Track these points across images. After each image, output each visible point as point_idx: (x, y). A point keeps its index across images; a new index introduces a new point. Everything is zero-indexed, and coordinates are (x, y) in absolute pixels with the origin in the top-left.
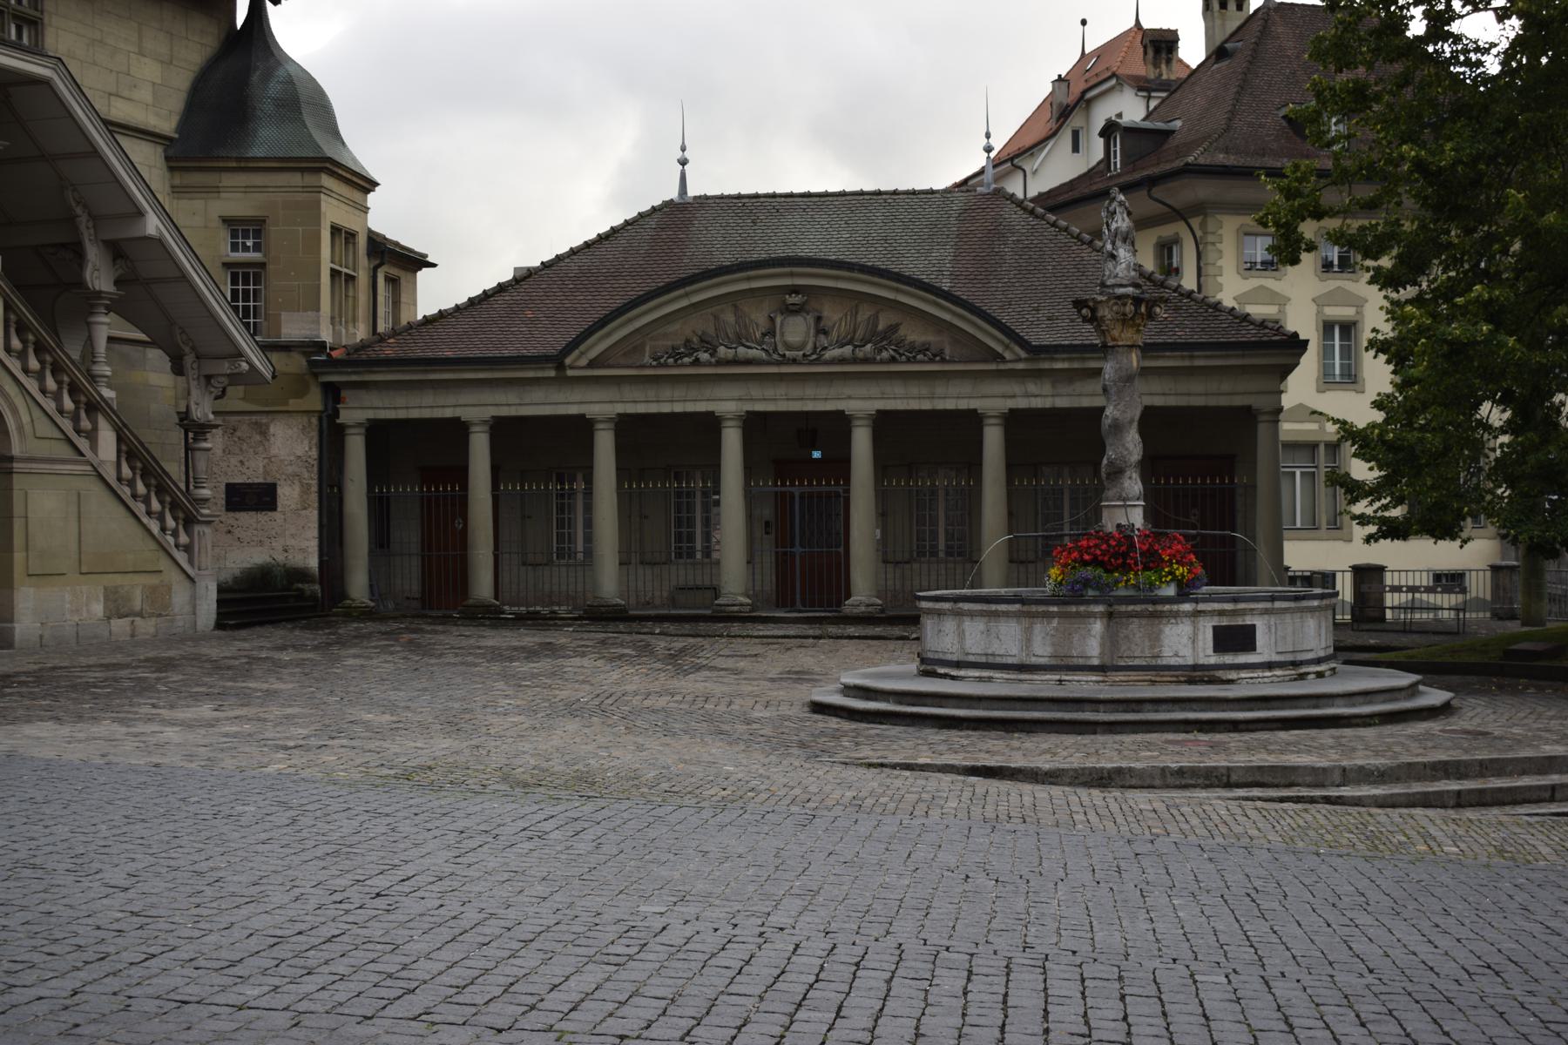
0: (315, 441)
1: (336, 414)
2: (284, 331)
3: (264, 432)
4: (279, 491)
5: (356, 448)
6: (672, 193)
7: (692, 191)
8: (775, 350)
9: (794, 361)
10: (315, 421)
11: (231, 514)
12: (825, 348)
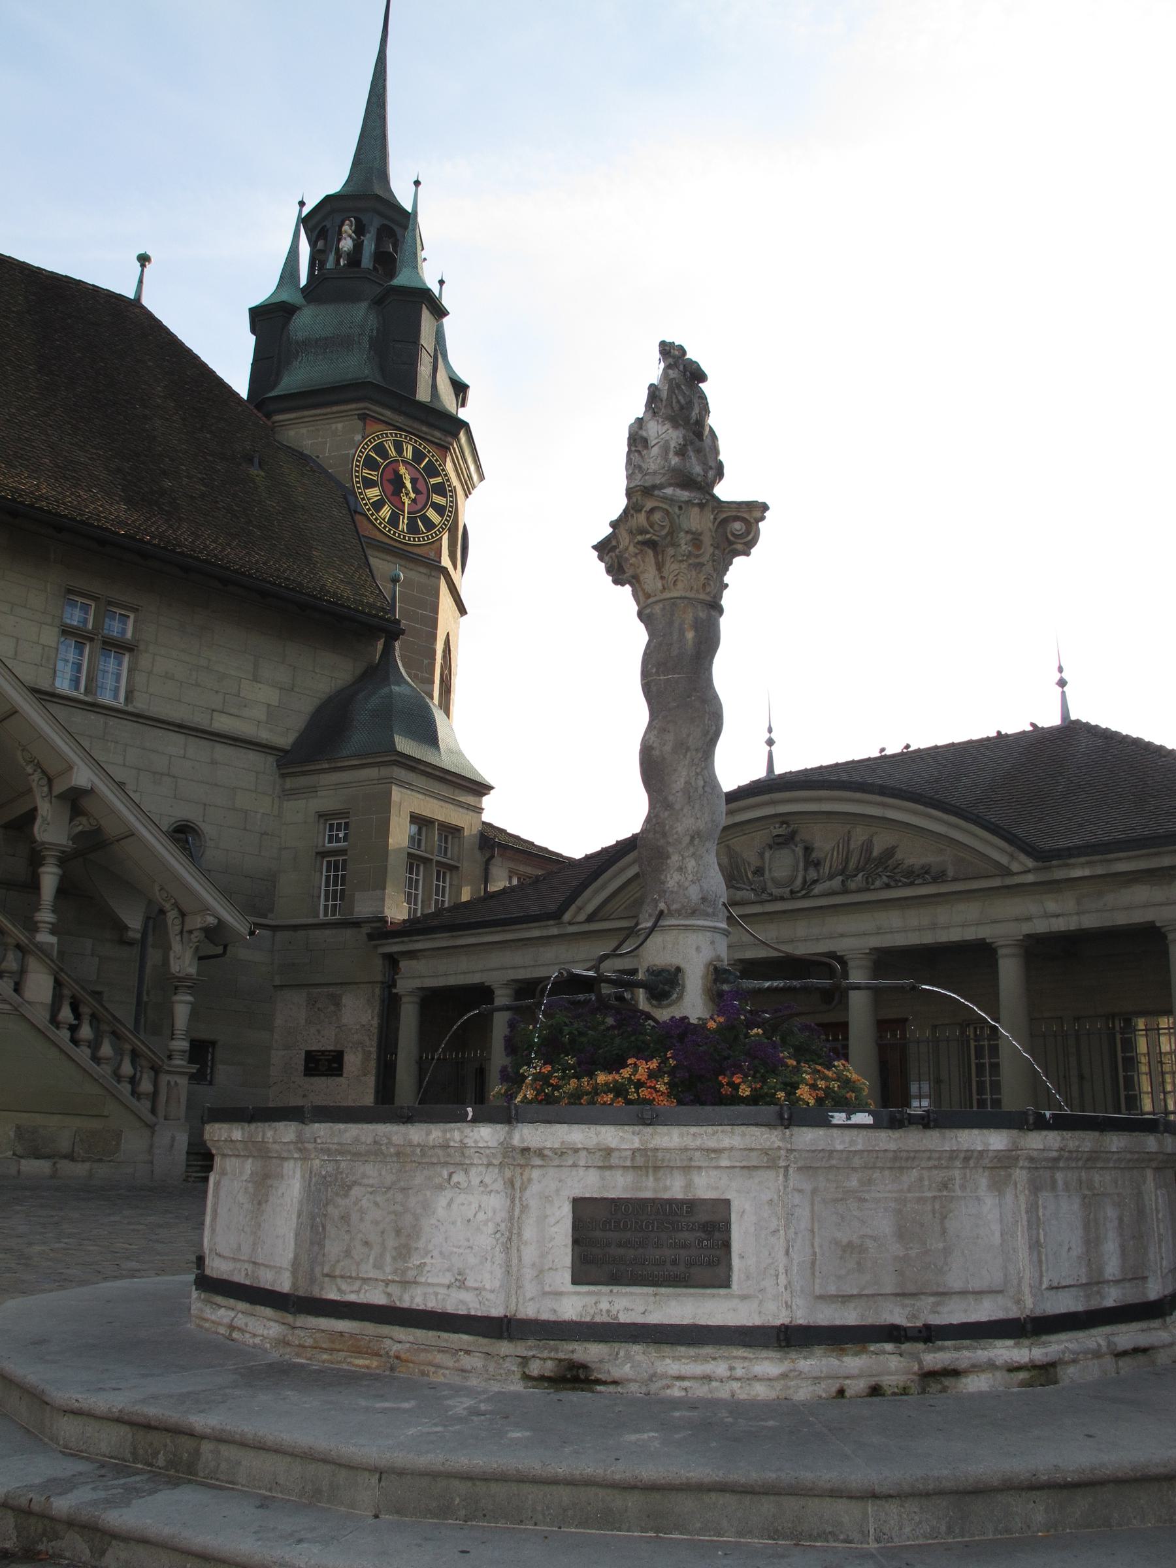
0: (377, 1010)
1: (394, 984)
2: (356, 909)
3: (336, 1002)
4: (346, 1058)
5: (409, 1016)
6: (760, 773)
7: (778, 771)
8: (764, 890)
9: (782, 899)
10: (377, 991)
11: (307, 1079)
12: (815, 882)
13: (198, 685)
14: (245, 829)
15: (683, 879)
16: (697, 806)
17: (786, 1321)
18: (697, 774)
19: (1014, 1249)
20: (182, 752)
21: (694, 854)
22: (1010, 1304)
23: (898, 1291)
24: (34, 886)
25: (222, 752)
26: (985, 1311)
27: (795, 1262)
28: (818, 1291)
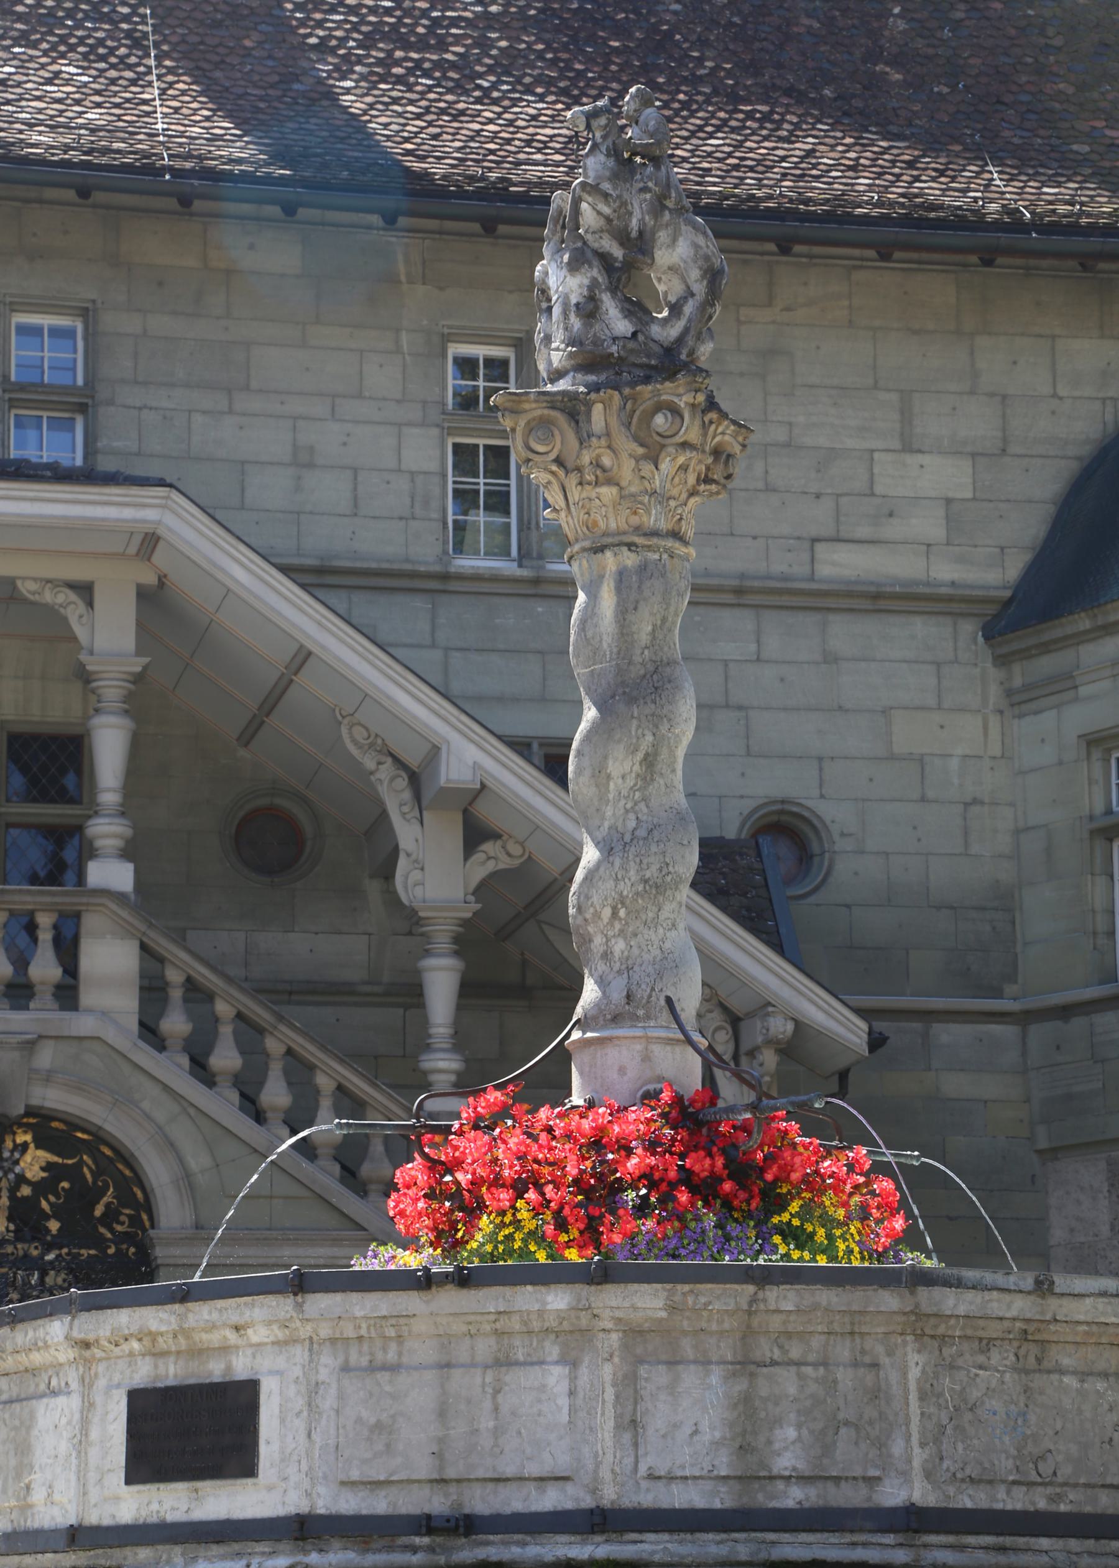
13: (769, 489)
14: (923, 799)
15: (607, 970)
16: (618, 863)
17: (304, 1508)
18: (627, 811)
19: (591, 1429)
20: (753, 647)
21: (621, 931)
22: (582, 1494)
23: (435, 1476)
24: (412, 994)
25: (845, 633)
26: (550, 1500)
27: (317, 1446)
28: (342, 1477)
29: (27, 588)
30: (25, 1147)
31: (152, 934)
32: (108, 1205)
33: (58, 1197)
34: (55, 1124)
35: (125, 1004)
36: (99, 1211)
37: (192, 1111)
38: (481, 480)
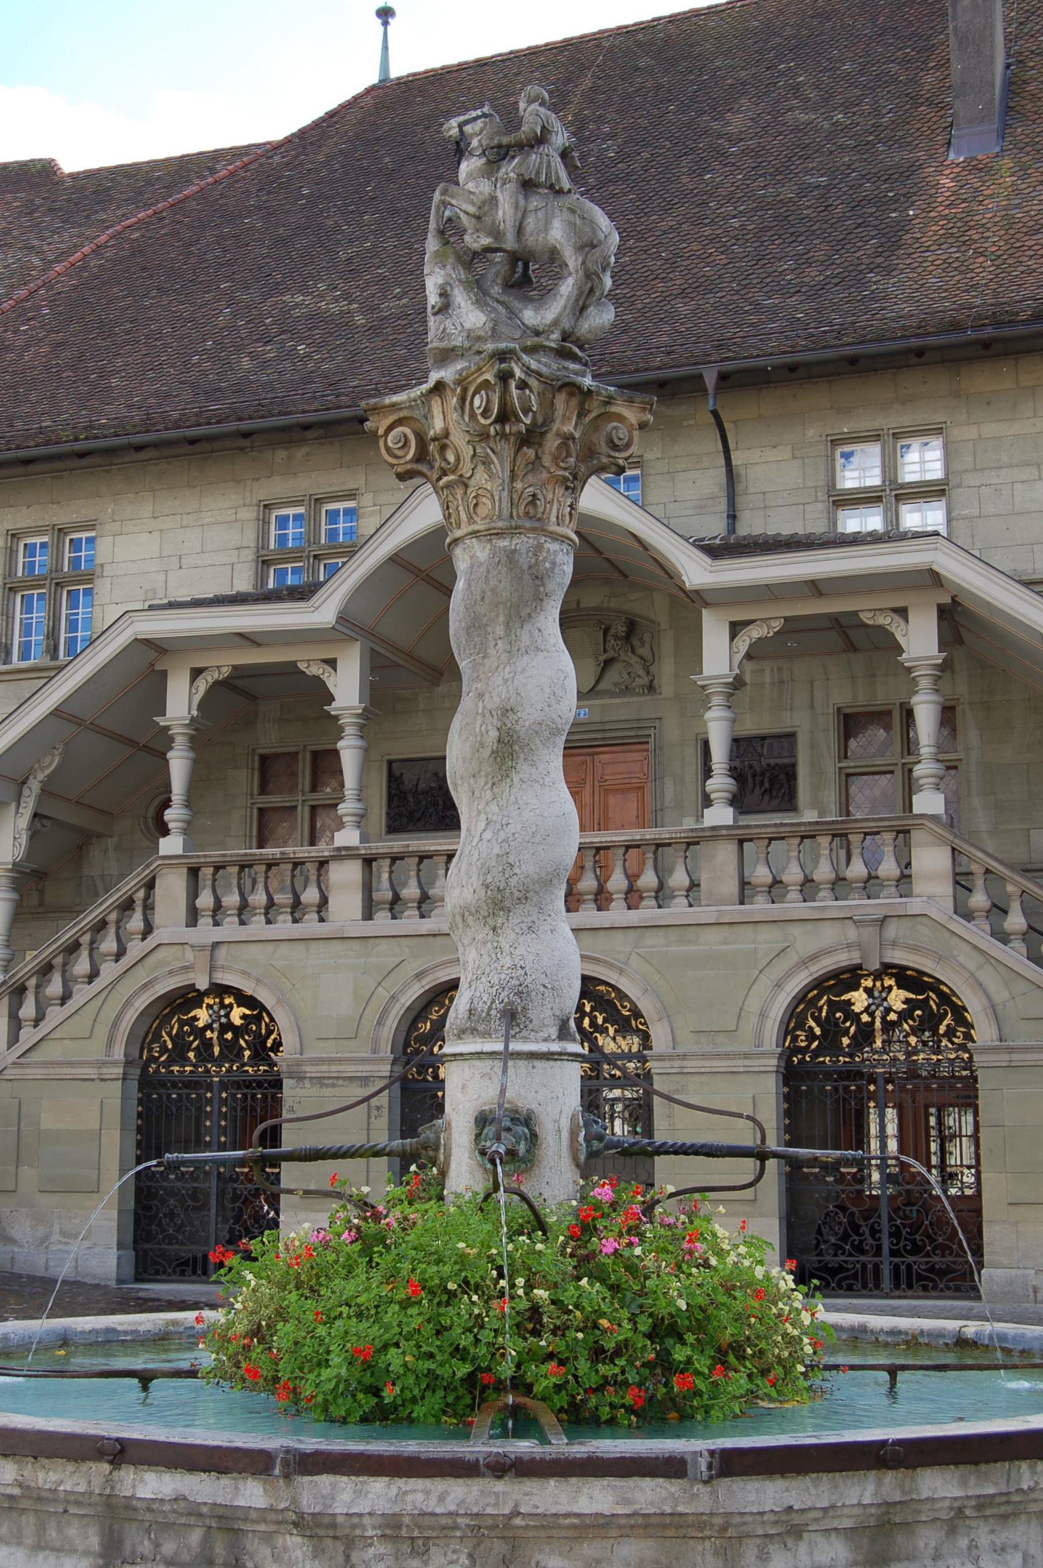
29: (866, 618)
30: (890, 988)
31: (958, 842)
32: (948, 1026)
33: (914, 1020)
34: (909, 973)
35: (945, 889)
36: (942, 1029)
37: (993, 962)
38: (83, 554)
